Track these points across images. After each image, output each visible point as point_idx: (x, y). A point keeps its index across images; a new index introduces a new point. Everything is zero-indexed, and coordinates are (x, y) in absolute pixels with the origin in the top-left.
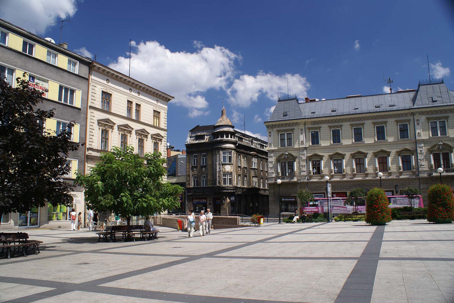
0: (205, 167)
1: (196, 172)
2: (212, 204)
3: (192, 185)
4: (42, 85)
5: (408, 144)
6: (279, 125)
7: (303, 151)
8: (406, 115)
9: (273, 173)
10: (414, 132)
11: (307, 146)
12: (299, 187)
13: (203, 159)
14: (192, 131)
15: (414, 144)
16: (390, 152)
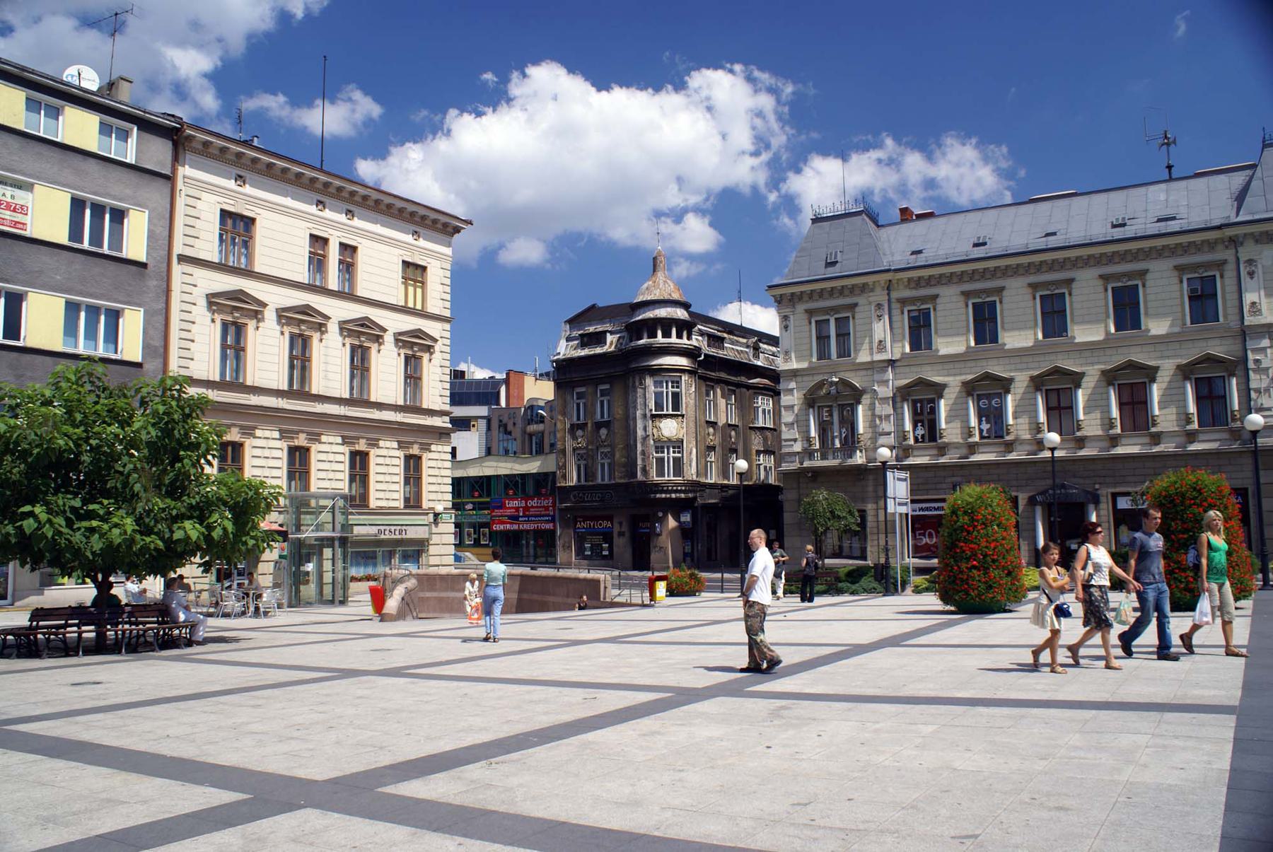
0: (607, 424)
1: (582, 442)
2: (627, 534)
3: (573, 480)
4: (13, 197)
5: (1217, 342)
6: (811, 295)
7: (884, 370)
8: (1212, 245)
9: (795, 440)
10: (1236, 303)
11: (897, 356)
12: (871, 483)
13: (602, 402)
14: (573, 322)
15: (1239, 340)
16: (1156, 369)
